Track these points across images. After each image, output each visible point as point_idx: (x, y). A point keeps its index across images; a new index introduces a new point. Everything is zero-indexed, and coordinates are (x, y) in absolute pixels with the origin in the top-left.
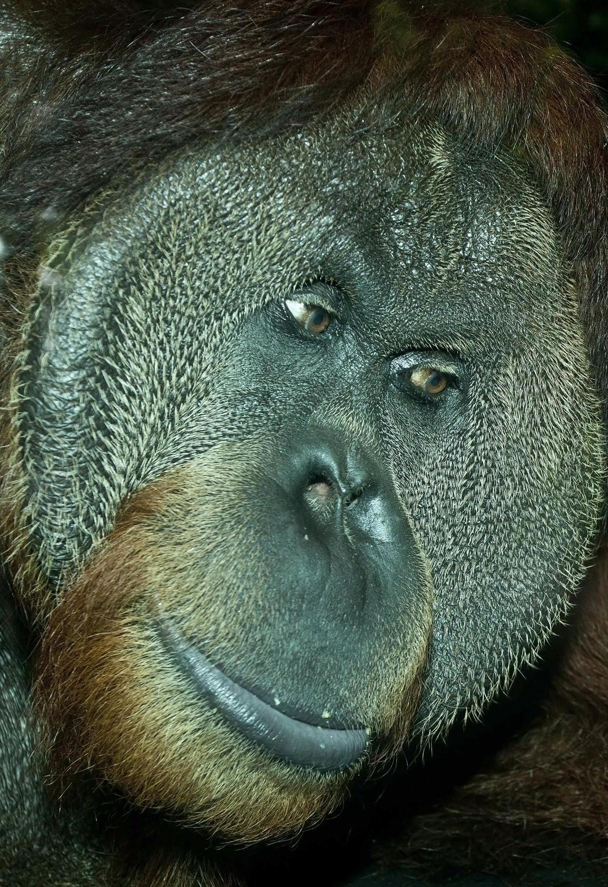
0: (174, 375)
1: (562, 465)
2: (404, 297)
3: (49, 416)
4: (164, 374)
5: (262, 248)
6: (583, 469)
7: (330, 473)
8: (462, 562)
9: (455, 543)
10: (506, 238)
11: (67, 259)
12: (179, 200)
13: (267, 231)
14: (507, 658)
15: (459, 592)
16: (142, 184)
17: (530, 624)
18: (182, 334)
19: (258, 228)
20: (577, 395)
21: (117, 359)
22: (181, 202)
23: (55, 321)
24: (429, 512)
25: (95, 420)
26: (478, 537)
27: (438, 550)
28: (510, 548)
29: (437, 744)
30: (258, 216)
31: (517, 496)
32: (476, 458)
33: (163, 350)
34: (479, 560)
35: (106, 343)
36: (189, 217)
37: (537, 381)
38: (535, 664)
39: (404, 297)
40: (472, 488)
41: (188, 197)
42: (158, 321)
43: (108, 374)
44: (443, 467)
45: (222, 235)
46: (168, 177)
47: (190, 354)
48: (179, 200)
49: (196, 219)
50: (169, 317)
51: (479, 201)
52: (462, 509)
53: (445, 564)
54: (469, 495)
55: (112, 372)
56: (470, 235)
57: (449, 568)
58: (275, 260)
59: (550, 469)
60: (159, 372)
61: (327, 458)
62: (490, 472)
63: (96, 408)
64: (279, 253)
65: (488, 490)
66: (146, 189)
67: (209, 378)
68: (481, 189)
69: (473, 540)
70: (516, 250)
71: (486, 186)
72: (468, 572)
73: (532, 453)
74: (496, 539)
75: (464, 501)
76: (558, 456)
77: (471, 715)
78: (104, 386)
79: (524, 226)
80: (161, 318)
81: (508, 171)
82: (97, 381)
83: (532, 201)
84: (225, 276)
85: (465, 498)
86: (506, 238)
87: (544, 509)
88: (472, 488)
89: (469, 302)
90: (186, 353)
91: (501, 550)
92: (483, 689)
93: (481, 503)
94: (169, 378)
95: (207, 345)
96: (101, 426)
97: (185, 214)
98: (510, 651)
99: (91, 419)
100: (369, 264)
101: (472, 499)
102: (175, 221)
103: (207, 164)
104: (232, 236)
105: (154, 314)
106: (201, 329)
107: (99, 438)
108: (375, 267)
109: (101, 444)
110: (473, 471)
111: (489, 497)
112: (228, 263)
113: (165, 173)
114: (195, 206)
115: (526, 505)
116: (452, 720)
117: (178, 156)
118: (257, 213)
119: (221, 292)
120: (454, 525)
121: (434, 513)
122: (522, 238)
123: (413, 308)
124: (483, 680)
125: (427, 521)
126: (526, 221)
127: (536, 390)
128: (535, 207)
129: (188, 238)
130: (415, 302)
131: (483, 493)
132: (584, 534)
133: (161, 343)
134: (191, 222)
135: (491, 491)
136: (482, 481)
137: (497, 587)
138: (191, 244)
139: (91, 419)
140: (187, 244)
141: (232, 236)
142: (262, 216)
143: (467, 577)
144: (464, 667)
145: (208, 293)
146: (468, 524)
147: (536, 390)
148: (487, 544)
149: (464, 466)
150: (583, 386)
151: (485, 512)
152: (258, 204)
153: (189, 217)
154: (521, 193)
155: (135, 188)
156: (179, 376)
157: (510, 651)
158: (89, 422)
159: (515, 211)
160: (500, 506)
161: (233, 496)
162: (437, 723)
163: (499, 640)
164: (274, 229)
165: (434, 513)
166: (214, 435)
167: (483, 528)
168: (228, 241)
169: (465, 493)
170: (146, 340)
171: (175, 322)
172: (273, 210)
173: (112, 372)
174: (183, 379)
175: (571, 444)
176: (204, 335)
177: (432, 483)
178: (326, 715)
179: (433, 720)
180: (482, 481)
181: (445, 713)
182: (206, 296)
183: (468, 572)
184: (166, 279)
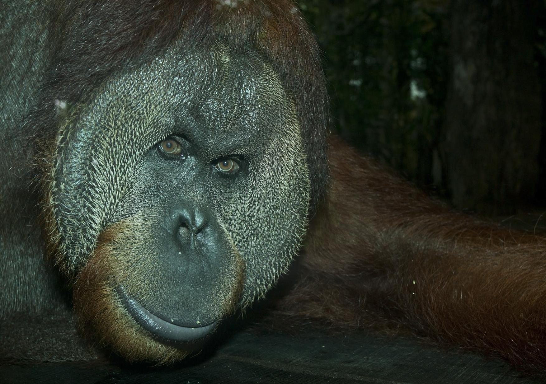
0: (118, 179)
1: (290, 186)
2: (215, 134)
3: (67, 210)
4: (114, 181)
5: (149, 116)
6: (299, 187)
7: (189, 222)
8: (251, 236)
9: (247, 229)
10: (258, 91)
11: (67, 140)
12: (111, 102)
13: (150, 108)
14: (273, 273)
15: (250, 248)
16: (94, 98)
17: (282, 258)
18: (120, 162)
19: (146, 107)
20: (296, 154)
21: (94, 181)
22: (112, 103)
23: (65, 169)
24: (236, 217)
25: (87, 209)
26: (256, 226)
27: (241, 232)
28: (270, 227)
29: (248, 309)
30: (145, 102)
31: (272, 206)
32: (253, 195)
33: (113, 170)
34: (257, 235)
35: (89, 175)
36: (116, 109)
37: (278, 155)
38: (287, 273)
39: (215, 134)
40: (252, 206)
41: (114, 100)
42: (110, 158)
43: (91, 188)
44: (239, 200)
45: (131, 113)
46: (104, 93)
47: (124, 171)
48: (111, 102)
49: (119, 109)
50: (114, 156)
51: (243, 75)
52: (249, 215)
53: (244, 238)
54: (251, 210)
55: (92, 187)
56: (242, 92)
57: (245, 239)
58: (155, 121)
59: (285, 189)
60: (111, 180)
61: (186, 214)
62: (259, 199)
63: (87, 204)
64: (157, 117)
65: (259, 206)
66: (96, 101)
67: (132, 181)
68: (244, 70)
69: (254, 227)
70: (264, 96)
71: (246, 68)
72: (253, 239)
73: (277, 186)
74: (264, 225)
75: (249, 212)
76: (288, 182)
77: (261, 297)
78: (90, 194)
79: (266, 83)
80: (111, 157)
81: (255, 59)
82: (86, 193)
83: (268, 71)
84: (135, 132)
85: (250, 211)
86: (258, 91)
87: (284, 208)
88: (252, 206)
89: (242, 130)
90: (122, 171)
91: (266, 229)
92: (265, 286)
93: (256, 212)
94: (116, 182)
95: (130, 166)
96: (90, 210)
97: (114, 108)
98: (274, 270)
99: (85, 209)
100: (197, 122)
101: (252, 211)
102: (111, 112)
103: (119, 83)
104: (135, 113)
105: (108, 156)
106: (128, 159)
107: (89, 216)
108: (200, 123)
109: (91, 218)
110: (252, 200)
111: (259, 209)
112: (136, 126)
113: (103, 91)
114: (118, 103)
115: (275, 209)
116: (253, 300)
117: (106, 82)
118: (144, 101)
119: (135, 140)
120: (246, 222)
121: (237, 218)
122: (266, 90)
123: (219, 138)
124: (264, 283)
125: (235, 221)
126: (267, 81)
127: (278, 158)
128: (269, 73)
129: (117, 118)
130: (220, 135)
131: (257, 208)
132: (302, 216)
133: (112, 168)
134: (118, 111)
135: (260, 207)
136: (256, 203)
137: (266, 244)
138: (119, 120)
139: (85, 209)
140: (117, 121)
141: (135, 113)
142: (146, 102)
143: (253, 242)
144: (255, 279)
145: (129, 141)
146: (252, 220)
147: (278, 158)
148: (260, 227)
149: (248, 198)
150: (298, 149)
151: (259, 215)
152: (144, 96)
153: (116, 109)
154: (262, 68)
155: (91, 102)
156: (120, 180)
157: (274, 270)
158: (84, 210)
159: (261, 77)
160: (265, 211)
161: (147, 237)
162: (247, 302)
163: (269, 266)
164: (153, 107)
165: (237, 218)
166: (138, 206)
167: (258, 221)
168: (134, 115)
169: (249, 209)
170: (105, 169)
171: (117, 158)
172: (151, 98)
173: (92, 187)
174: (122, 181)
175: (293, 176)
176: (130, 161)
177: (235, 206)
178: (198, 322)
179: (245, 301)
180: (256, 203)
181: (249, 298)
182: (129, 143)
183: (253, 239)
184: (111, 139)
